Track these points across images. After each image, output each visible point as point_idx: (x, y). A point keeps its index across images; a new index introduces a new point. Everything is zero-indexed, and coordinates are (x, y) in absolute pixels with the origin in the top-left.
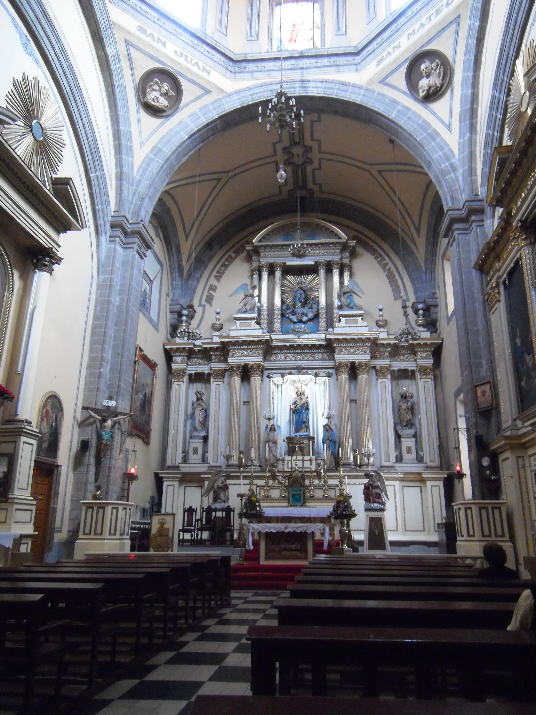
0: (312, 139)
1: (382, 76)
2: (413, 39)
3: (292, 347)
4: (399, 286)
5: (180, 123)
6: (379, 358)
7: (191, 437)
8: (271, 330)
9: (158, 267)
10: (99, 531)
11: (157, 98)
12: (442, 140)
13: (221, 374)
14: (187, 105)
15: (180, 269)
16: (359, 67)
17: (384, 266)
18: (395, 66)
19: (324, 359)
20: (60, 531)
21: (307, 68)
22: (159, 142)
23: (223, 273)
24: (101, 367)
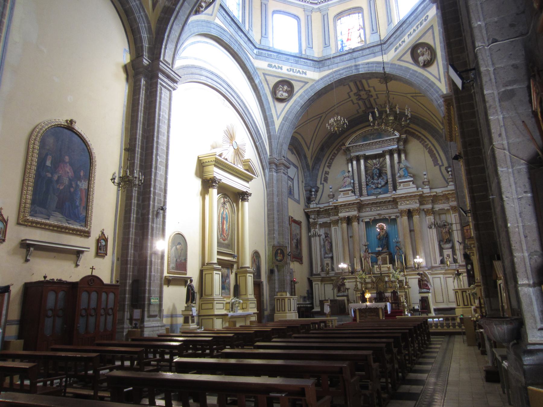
0: (369, 87)
1: (399, 57)
2: (411, 38)
4: (436, 158)
5: (295, 101)
6: (426, 204)
7: (325, 258)
8: (361, 195)
9: (296, 170)
10: (283, 309)
11: (282, 94)
12: (437, 87)
13: (336, 223)
14: (297, 92)
15: (308, 165)
17: (426, 146)
20: (267, 310)
22: (286, 114)
23: (332, 163)
24: (274, 233)
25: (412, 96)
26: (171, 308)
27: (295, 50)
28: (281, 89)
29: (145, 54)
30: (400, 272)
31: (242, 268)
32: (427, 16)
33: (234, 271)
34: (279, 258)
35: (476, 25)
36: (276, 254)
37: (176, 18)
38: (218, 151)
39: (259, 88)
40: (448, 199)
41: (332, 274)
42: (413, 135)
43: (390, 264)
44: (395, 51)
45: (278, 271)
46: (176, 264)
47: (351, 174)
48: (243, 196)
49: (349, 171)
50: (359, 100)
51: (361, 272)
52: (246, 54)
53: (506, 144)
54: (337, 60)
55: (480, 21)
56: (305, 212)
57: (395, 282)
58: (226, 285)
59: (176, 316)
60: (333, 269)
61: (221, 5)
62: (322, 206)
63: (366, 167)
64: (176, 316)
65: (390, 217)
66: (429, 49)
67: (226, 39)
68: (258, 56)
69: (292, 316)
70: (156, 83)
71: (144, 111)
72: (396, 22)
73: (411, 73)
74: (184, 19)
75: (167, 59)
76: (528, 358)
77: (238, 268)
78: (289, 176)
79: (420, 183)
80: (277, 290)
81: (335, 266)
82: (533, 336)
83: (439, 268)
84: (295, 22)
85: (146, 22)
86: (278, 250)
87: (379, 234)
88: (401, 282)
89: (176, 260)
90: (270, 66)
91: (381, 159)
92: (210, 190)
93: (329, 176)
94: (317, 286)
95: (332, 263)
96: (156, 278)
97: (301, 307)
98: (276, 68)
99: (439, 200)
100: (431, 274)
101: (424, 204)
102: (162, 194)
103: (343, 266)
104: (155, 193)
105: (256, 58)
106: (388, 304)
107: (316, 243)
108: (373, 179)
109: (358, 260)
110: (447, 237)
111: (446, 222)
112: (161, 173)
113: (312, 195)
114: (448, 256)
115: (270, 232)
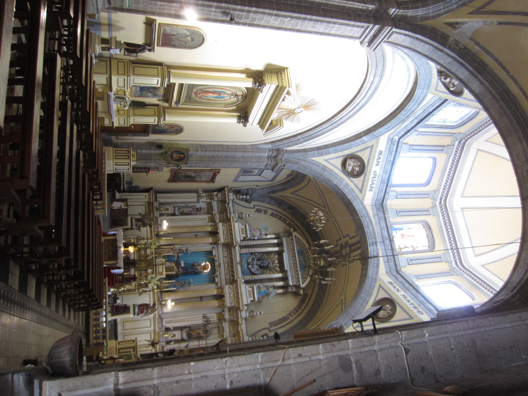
1: (383, 286)
3: (232, 259)
5: (342, 179)
6: (229, 314)
7: (174, 207)
8: (241, 247)
9: (270, 179)
10: (117, 157)
11: (350, 165)
13: (212, 220)
14: (352, 181)
15: (274, 192)
16: (389, 273)
17: (290, 314)
18: (388, 291)
19: (226, 280)
20: (117, 139)
21: (384, 244)
22: (330, 169)
23: (275, 217)
24: (202, 151)
25: (342, 300)
26: (119, 25)
27: (394, 180)
28: (356, 164)
29: (401, 12)
30: (157, 285)
31: (164, 112)
32: (422, 314)
33: (160, 103)
34: (175, 155)
35: (425, 332)
36: (179, 152)
37: (436, 48)
38: (292, 90)
39: (358, 141)
40: (234, 336)
41: (157, 214)
42: (302, 302)
43: (167, 275)
44: (389, 282)
45: (160, 154)
46: (170, 35)
47: (264, 237)
48: (244, 116)
49: (266, 235)
50: (341, 247)
51: (157, 244)
52: (393, 128)
53: (289, 363)
54: (383, 224)
55: (429, 336)
56: (224, 187)
57: (146, 280)
58: (145, 93)
59: (110, 30)
60: (161, 215)
61: (446, 100)
62: (231, 205)
63: (271, 253)
64: (110, 30)
65: (217, 276)
66: (389, 315)
67: (411, 105)
68: (391, 141)
69: (110, 166)
70: (369, 22)
71: (340, 6)
72: (418, 283)
73: (366, 298)
74: (434, 58)
75: (394, 35)
76: (21, 380)
77: (164, 108)
78: (263, 171)
79: (252, 308)
80: (139, 151)
81: (165, 217)
82: (51, 387)
83: (160, 326)
84: (424, 181)
85: (434, 14)
86: (184, 154)
87: (199, 265)
88: (146, 285)
89: (174, 35)
90: (381, 153)
91: (278, 269)
92: (251, 80)
93: (262, 214)
94: (143, 197)
95: (168, 215)
96: (153, 6)
97: (120, 178)
98: (378, 160)
99: (233, 327)
100: (154, 318)
101: (229, 311)
102: (248, 21)
103: (165, 225)
104: (249, 12)
105: (389, 138)
106: (122, 271)
107: (191, 198)
108: (258, 260)
109: (170, 242)
110: (194, 335)
111: (210, 334)
112: (272, 21)
113: (243, 195)
114: (174, 336)
115: (204, 147)
